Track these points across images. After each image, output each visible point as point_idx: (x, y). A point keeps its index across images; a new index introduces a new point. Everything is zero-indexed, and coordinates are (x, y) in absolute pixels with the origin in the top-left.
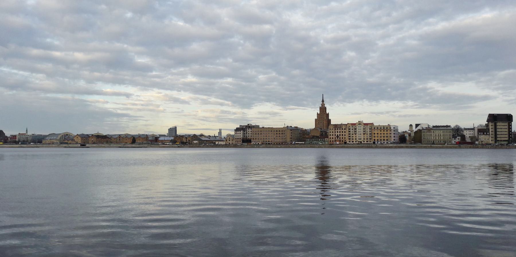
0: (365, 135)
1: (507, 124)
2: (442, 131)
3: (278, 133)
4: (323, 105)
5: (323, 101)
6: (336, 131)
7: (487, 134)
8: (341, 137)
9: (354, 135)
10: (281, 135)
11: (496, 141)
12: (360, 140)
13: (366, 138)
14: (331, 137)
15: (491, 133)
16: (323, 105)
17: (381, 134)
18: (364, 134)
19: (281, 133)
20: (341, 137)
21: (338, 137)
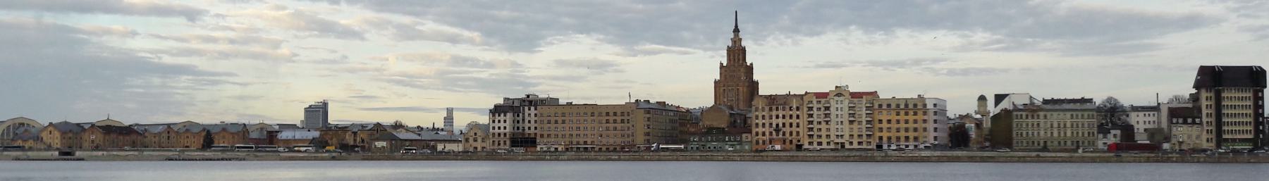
0: (855, 126)
1: (1250, 94)
2: (1068, 114)
3: (611, 118)
4: (737, 40)
5: (736, 30)
6: (774, 113)
7: (1194, 123)
8: (787, 129)
9: (823, 126)
10: (619, 126)
11: (1220, 141)
12: (840, 140)
13: (856, 133)
14: (760, 130)
15: (1205, 119)
16: (737, 40)
17: (898, 122)
18: (851, 122)
19: (619, 119)
20: (787, 129)
21: (777, 130)
